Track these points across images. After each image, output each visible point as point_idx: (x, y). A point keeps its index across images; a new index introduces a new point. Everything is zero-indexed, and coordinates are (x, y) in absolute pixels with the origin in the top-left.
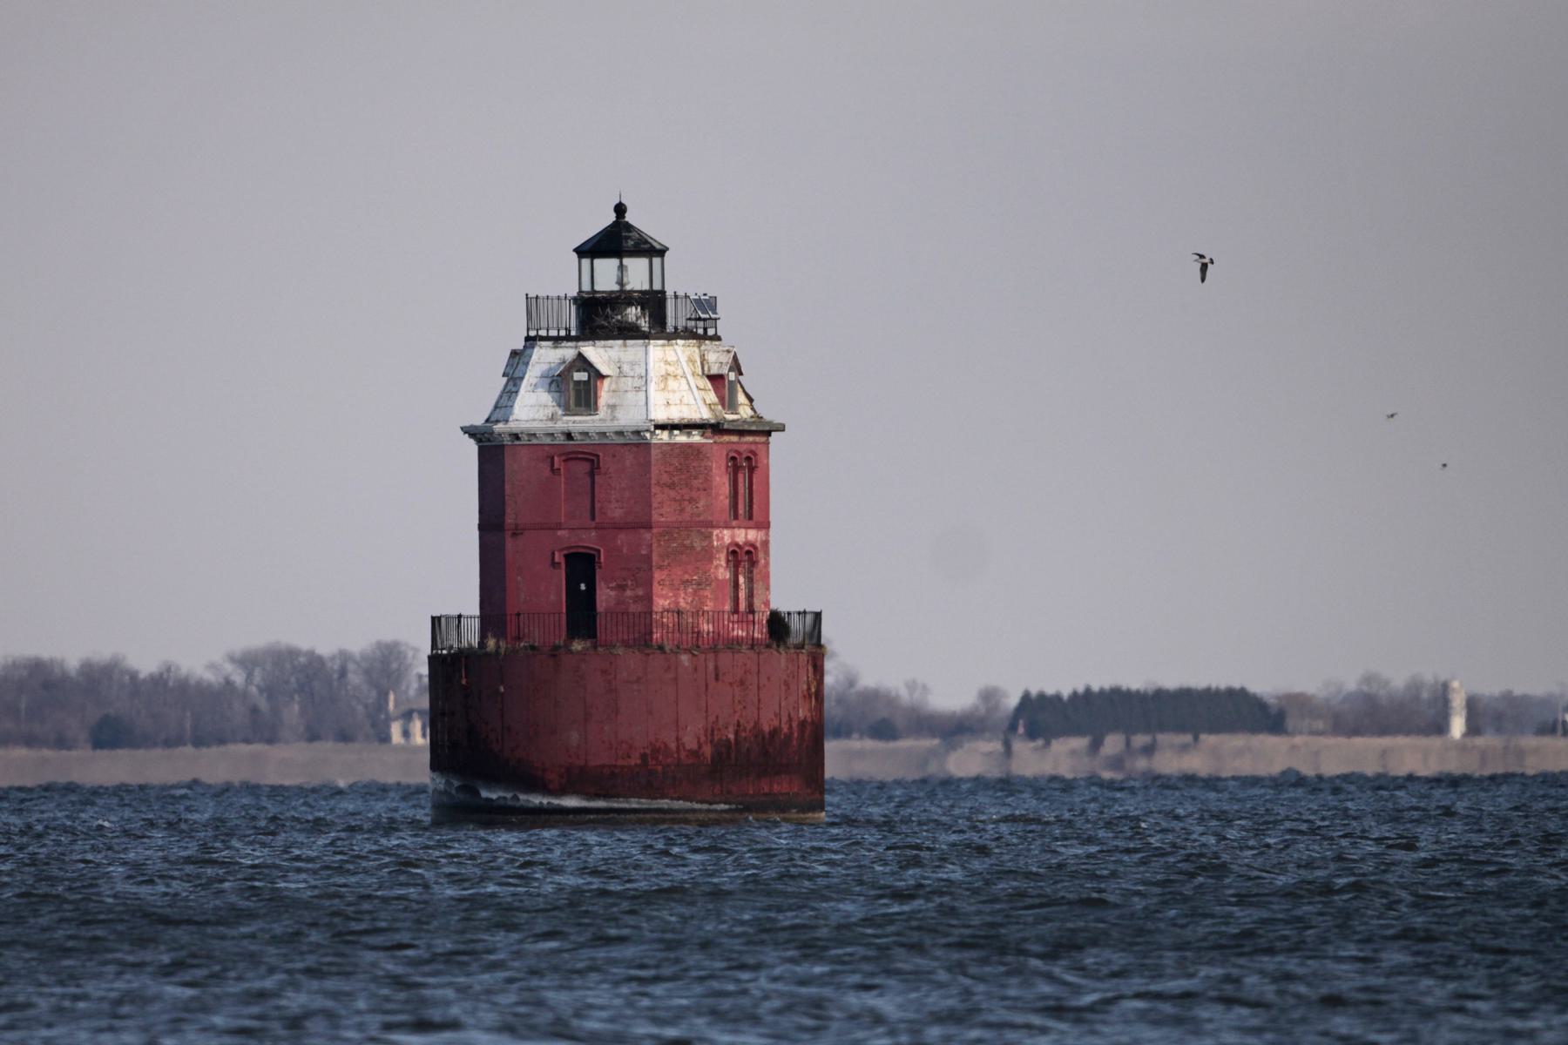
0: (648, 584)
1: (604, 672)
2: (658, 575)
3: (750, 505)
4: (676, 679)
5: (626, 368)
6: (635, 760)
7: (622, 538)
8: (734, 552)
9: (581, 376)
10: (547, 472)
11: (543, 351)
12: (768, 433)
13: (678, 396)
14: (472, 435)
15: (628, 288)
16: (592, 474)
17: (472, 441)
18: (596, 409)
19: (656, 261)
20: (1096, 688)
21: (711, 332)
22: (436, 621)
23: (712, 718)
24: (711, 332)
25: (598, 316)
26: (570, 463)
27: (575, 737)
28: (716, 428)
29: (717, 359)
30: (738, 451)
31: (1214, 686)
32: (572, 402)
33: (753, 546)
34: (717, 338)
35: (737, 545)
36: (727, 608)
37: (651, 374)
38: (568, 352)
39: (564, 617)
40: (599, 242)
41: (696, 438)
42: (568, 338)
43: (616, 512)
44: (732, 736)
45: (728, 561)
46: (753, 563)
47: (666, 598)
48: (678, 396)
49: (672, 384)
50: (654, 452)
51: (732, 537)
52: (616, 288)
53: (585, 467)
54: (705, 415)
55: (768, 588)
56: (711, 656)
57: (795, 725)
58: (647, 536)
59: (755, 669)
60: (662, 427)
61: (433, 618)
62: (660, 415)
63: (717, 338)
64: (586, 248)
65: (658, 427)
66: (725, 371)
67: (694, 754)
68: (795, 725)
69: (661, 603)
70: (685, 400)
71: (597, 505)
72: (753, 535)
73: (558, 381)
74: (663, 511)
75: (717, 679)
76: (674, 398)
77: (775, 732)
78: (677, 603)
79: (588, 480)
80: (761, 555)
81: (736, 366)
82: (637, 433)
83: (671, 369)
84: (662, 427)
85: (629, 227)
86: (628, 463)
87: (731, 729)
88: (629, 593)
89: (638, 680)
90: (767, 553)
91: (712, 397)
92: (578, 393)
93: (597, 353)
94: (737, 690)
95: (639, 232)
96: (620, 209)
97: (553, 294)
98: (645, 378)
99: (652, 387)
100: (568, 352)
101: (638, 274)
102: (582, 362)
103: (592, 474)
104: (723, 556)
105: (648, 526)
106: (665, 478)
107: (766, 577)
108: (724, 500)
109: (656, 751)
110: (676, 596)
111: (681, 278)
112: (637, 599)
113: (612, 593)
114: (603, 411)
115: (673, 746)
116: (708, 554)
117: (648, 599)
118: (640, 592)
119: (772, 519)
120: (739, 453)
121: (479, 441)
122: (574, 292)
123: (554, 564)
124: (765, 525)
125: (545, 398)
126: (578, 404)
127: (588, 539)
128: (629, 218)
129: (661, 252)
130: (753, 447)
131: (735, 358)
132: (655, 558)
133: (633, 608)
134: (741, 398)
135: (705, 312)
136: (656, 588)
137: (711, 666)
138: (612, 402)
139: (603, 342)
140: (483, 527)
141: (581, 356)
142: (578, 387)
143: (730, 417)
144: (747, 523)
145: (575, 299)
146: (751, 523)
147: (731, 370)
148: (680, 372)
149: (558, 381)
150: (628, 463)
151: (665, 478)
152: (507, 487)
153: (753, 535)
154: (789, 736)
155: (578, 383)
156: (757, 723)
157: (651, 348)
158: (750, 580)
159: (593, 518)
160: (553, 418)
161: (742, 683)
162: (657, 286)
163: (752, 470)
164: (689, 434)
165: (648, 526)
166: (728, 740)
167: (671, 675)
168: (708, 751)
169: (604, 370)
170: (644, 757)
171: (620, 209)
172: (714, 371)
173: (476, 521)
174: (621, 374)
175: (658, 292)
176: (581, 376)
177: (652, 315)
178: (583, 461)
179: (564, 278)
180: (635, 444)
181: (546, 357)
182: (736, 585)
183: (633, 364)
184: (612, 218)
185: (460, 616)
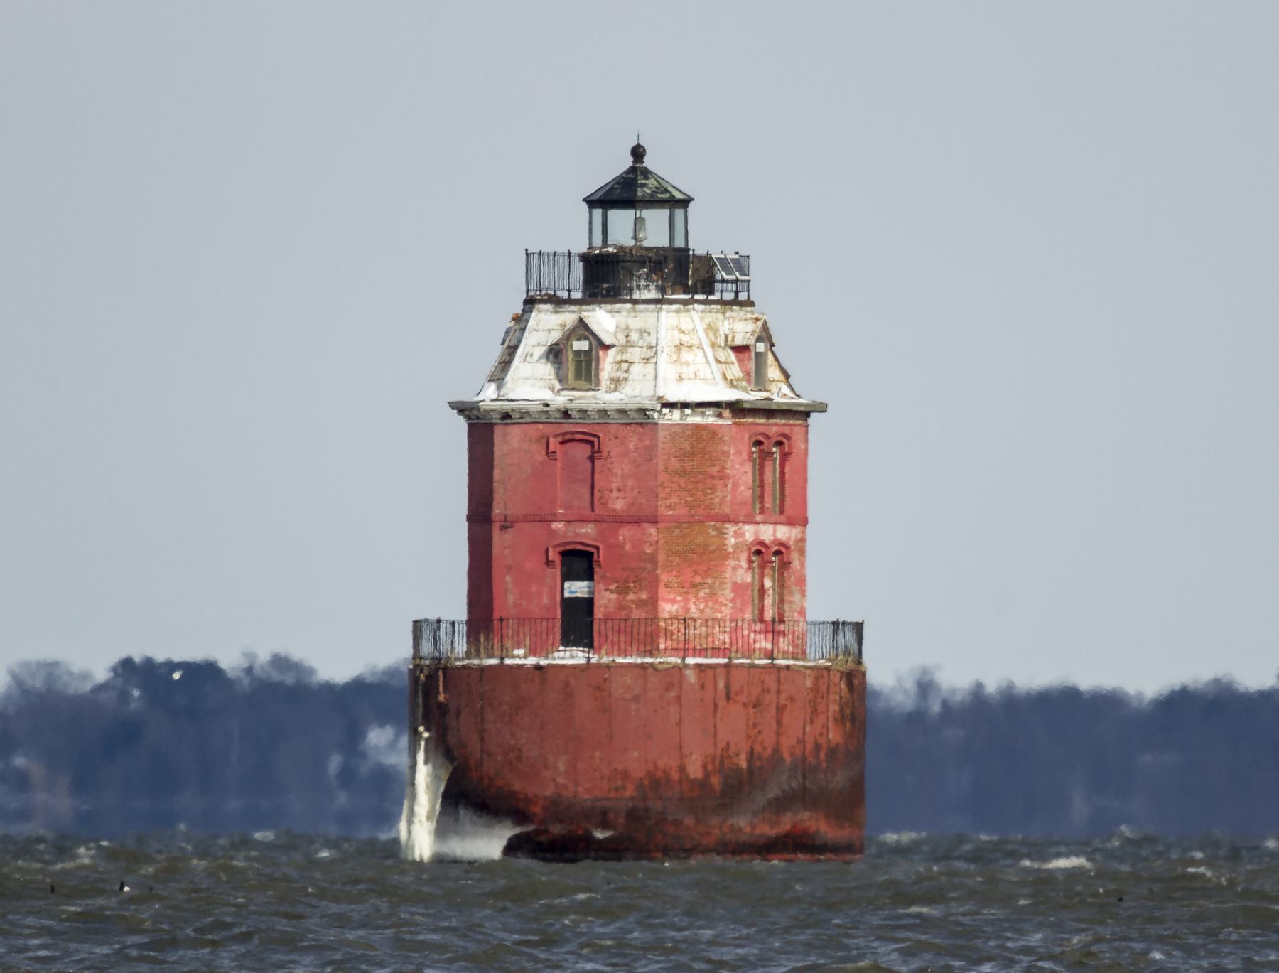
3: (784, 496)
4: (679, 698)
5: (634, 337)
7: (625, 534)
8: (758, 552)
9: (582, 345)
10: (540, 456)
11: (542, 315)
13: (691, 370)
14: (461, 412)
15: (646, 244)
17: (461, 418)
18: (598, 383)
19: (679, 213)
20: (229, 660)
21: (743, 296)
22: (417, 626)
23: (721, 745)
24: (743, 296)
25: (605, 275)
26: (567, 445)
28: (736, 408)
29: (740, 327)
30: (774, 432)
31: (992, 686)
32: (571, 375)
33: (783, 545)
34: (750, 303)
35: (762, 543)
36: (748, 616)
37: (662, 343)
38: (568, 317)
39: (558, 623)
40: (612, 189)
41: (709, 418)
42: (570, 301)
43: (619, 504)
44: (744, 765)
45: (750, 562)
46: (785, 565)
47: (673, 601)
48: (691, 370)
49: (686, 355)
50: (661, 434)
51: (756, 533)
52: (631, 243)
53: (587, 450)
55: (803, 594)
59: (774, 687)
61: (415, 622)
63: (750, 303)
64: (595, 197)
65: (665, 405)
66: (751, 341)
67: (704, 784)
69: (667, 608)
70: (701, 375)
71: (597, 494)
72: (783, 532)
73: (555, 353)
74: (670, 505)
75: (728, 698)
76: (686, 371)
78: (687, 610)
79: (589, 465)
80: (795, 556)
81: (765, 335)
82: (642, 411)
83: (685, 339)
84: (672, 406)
85: (646, 173)
86: (631, 446)
87: (743, 756)
88: (631, 597)
89: (636, 699)
90: (802, 552)
91: (735, 371)
92: (578, 364)
93: (603, 320)
94: (752, 711)
95: (658, 179)
97: (562, 249)
99: (663, 359)
100: (568, 317)
101: (656, 230)
102: (583, 330)
103: (592, 459)
104: (743, 557)
107: (801, 581)
108: (745, 492)
110: (686, 601)
111: (705, 237)
112: (640, 604)
113: (614, 596)
115: (675, 775)
117: (653, 603)
118: (644, 596)
119: (811, 513)
120: (768, 437)
121: (469, 418)
122: (583, 249)
123: (549, 563)
124: (801, 520)
126: (578, 376)
127: (587, 533)
128: (648, 162)
129: (685, 203)
130: (786, 430)
131: (765, 327)
132: (661, 557)
133: (636, 614)
134: (773, 372)
135: (729, 272)
136: (662, 591)
138: (615, 375)
139: (609, 307)
140: (471, 518)
141: (581, 320)
142: (577, 359)
144: (777, 517)
145: (585, 258)
146: (783, 518)
147: (759, 339)
148: (695, 342)
149: (555, 353)
150: (631, 446)
152: (496, 472)
153: (783, 532)
155: (578, 353)
156: (682, 769)
157: (663, 314)
158: (781, 584)
159: (593, 510)
162: (679, 243)
163: (785, 456)
164: (703, 414)
166: (739, 769)
167: (673, 694)
168: (716, 781)
170: (640, 785)
172: (739, 341)
173: (466, 512)
174: (629, 343)
175: (680, 250)
176: (582, 345)
177: (686, 274)
178: (579, 438)
179: (573, 233)
180: (640, 419)
181: (547, 325)
182: (762, 591)
183: (642, 332)
184: (628, 162)
185: (439, 621)
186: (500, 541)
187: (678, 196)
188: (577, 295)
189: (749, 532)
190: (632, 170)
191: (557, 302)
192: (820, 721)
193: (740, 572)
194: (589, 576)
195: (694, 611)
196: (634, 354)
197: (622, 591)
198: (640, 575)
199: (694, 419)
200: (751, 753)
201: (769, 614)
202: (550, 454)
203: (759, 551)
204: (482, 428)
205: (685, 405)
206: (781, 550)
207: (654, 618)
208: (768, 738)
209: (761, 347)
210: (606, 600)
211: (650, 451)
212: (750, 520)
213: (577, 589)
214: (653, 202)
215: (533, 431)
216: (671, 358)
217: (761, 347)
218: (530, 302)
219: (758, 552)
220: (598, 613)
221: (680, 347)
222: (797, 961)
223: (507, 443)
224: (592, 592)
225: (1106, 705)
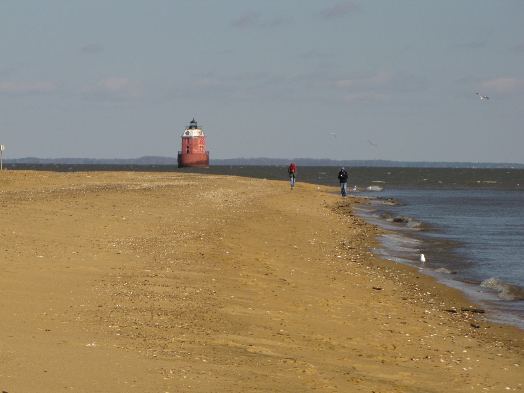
25: (191, 128)
74: (194, 143)
93: (189, 131)
142: (188, 133)
177: (196, 127)
179: (189, 125)
180: (191, 138)
181: (186, 131)
193: (199, 148)
198: (192, 148)
203: (201, 147)
216: (195, 133)
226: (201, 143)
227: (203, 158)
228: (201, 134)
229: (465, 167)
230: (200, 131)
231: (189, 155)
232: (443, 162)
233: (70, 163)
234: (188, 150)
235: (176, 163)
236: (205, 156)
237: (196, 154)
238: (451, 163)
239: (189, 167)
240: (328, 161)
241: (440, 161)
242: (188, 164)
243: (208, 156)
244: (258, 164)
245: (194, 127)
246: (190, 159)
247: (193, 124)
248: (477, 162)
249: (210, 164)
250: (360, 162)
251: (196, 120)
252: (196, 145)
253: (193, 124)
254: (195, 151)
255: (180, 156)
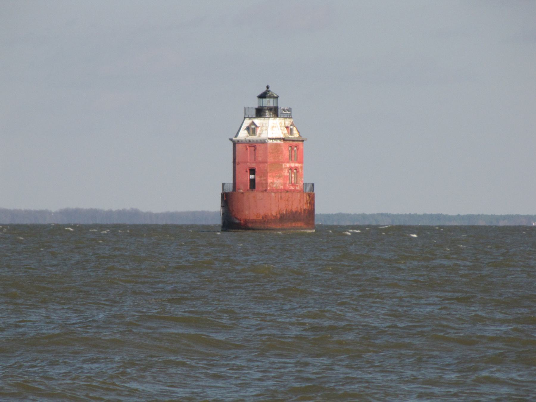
0: (267, 176)
1: (254, 197)
2: (269, 174)
6: (261, 218)
7: (261, 165)
9: (253, 127)
12: (303, 141)
16: (255, 150)
25: (260, 112)
27: (247, 213)
28: (284, 139)
36: (288, 182)
41: (279, 142)
43: (260, 159)
44: (285, 213)
45: (288, 171)
54: (282, 136)
56: (280, 194)
57: (302, 210)
58: (266, 165)
60: (270, 139)
62: (270, 136)
66: (289, 126)
67: (276, 217)
68: (302, 210)
69: (270, 181)
73: (248, 129)
74: (270, 159)
77: (296, 212)
80: (300, 171)
83: (274, 125)
84: (270, 139)
85: (269, 91)
93: (257, 121)
96: (268, 87)
97: (250, 107)
98: (267, 127)
102: (253, 123)
103: (255, 150)
105: (266, 162)
106: (271, 151)
109: (266, 216)
112: (264, 180)
114: (257, 135)
115: (270, 215)
116: (282, 169)
117: (266, 180)
122: (257, 107)
123: (247, 171)
125: (246, 132)
127: (254, 166)
128: (270, 89)
129: (277, 97)
136: (268, 177)
137: (280, 196)
142: (252, 129)
143: (290, 137)
149: (248, 129)
151: (271, 151)
154: (301, 212)
156: (271, 213)
160: (247, 137)
161: (287, 200)
165: (266, 162)
168: (279, 216)
169: (258, 125)
170: (263, 218)
171: (268, 87)
172: (287, 126)
174: (263, 126)
176: (253, 127)
177: (275, 112)
178: (253, 145)
179: (255, 103)
180: (263, 142)
181: (247, 122)
183: (266, 124)
186: (237, 167)
187: (275, 96)
188: (254, 116)
189: (288, 165)
190: (267, 91)
191: (250, 118)
192: (301, 204)
193: (286, 173)
194: (254, 174)
195: (275, 182)
196: (264, 128)
197: (261, 177)
198: (265, 174)
199: (275, 142)
200: (286, 210)
201: (293, 182)
202: (247, 149)
203: (291, 169)
204: (235, 144)
205: (273, 139)
206: (296, 169)
207: (267, 183)
208: (290, 207)
209: (292, 127)
210: (257, 180)
211: (266, 148)
212: (288, 163)
213: (252, 177)
214: (270, 97)
215: (244, 145)
216: (272, 129)
217: (292, 127)
218: (245, 118)
219: (291, 169)
220: (256, 181)
221: (273, 127)
222: (512, 326)
223: (239, 147)
224: (254, 177)
225: (473, 215)
226: (291, 158)
227: (298, 204)
228: (291, 132)
229: (431, 224)
230: (288, 122)
231: (258, 194)
232: (382, 214)
233: (329, 223)
234: (253, 181)
235: (219, 222)
236: (306, 198)
237: (277, 191)
238: (398, 215)
239: (248, 229)
240: (135, 213)
241: (375, 211)
242: (254, 222)
243: (311, 197)
244: (204, 223)
245: (270, 109)
246: (255, 207)
247: (268, 103)
248: (422, 214)
249: (317, 222)
250: (43, 213)
251: (274, 90)
252: (278, 165)
253: (268, 103)
254: (275, 181)
255: (227, 199)
